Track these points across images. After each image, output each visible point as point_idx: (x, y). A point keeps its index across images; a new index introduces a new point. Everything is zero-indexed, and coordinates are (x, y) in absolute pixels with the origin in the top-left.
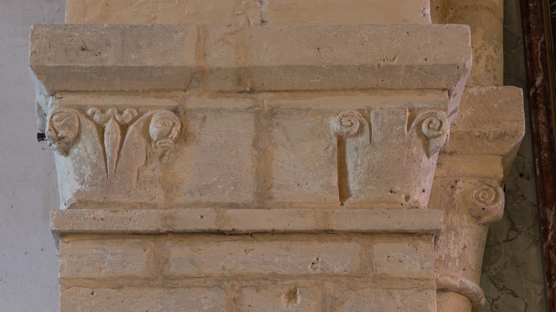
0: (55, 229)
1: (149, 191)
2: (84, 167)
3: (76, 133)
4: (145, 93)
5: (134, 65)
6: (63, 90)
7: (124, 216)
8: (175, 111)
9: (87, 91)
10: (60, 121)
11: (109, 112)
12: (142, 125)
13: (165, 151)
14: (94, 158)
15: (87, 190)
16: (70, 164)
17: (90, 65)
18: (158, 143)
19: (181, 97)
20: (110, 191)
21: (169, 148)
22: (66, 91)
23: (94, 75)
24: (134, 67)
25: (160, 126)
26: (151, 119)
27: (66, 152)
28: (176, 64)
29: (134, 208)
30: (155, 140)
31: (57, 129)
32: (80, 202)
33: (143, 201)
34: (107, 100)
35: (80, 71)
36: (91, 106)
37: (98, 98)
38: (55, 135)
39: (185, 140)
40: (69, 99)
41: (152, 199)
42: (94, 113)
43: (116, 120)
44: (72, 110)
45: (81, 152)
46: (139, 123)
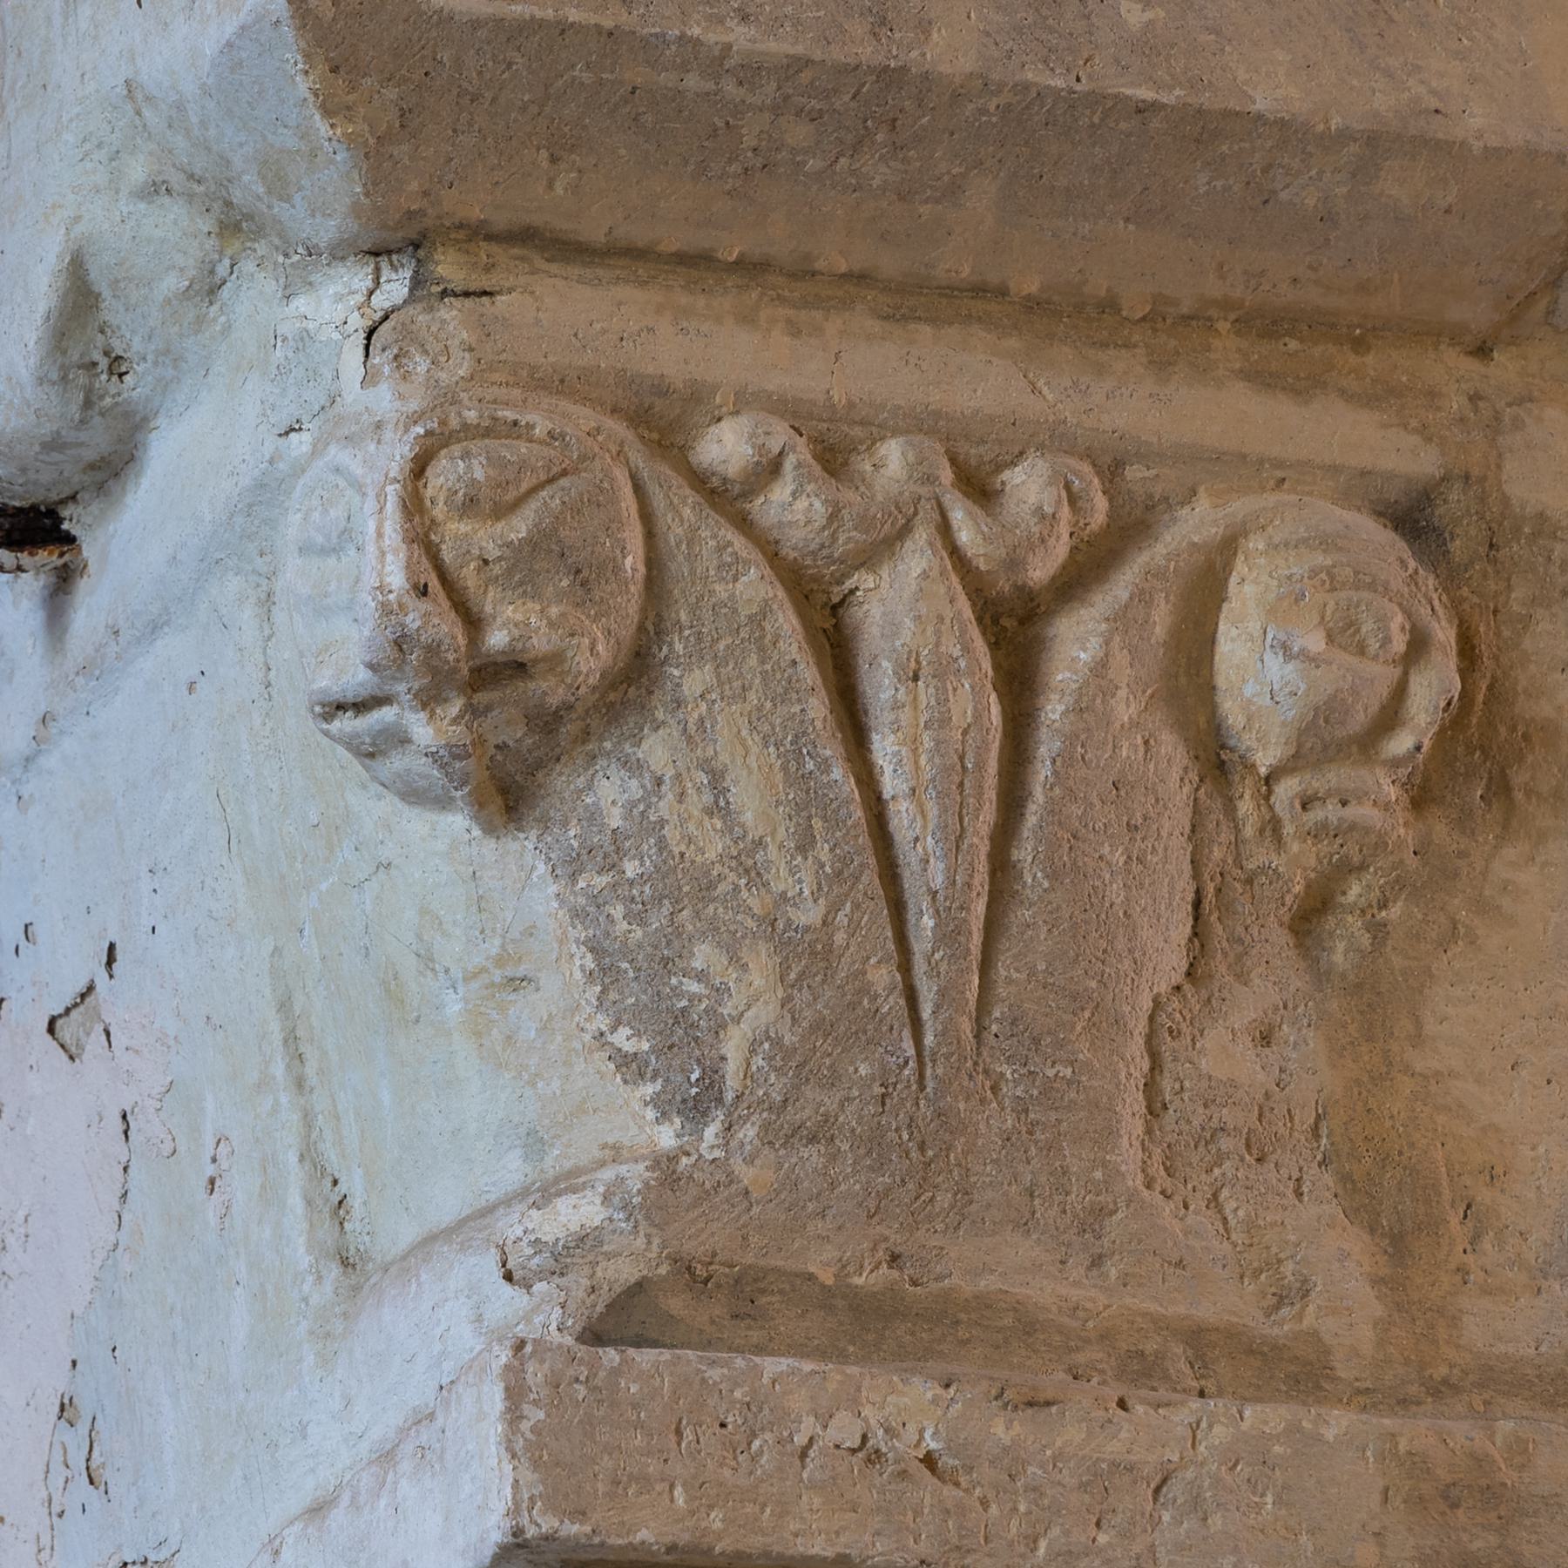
0: (548, 1524)
1: (1250, 1226)
2: (704, 955)
3: (627, 632)
4: (1172, 332)
5: (1145, 94)
6: (502, 220)
7: (1114, 1449)
8: (1412, 519)
9: (695, 263)
10: (501, 511)
11: (893, 460)
12: (1161, 619)
13: (1346, 869)
14: (796, 882)
15: (746, 1174)
16: (543, 900)
17: (779, 47)
18: (1287, 789)
19: (1456, 403)
20: (944, 1200)
21: (1381, 845)
22: (525, 237)
23: (799, 133)
24: (1143, 109)
25: (1315, 642)
26: (1228, 567)
27: (507, 794)
28: (1477, 121)
29: (1142, 1369)
30: (1264, 760)
31: (469, 577)
32: (692, 1275)
33: (1206, 1312)
34: (864, 364)
35: (692, 82)
36: (743, 401)
37: (794, 331)
38: (462, 641)
39: (1500, 788)
40: (558, 312)
41: (1281, 1300)
42: (773, 468)
43: (955, 552)
44: (585, 417)
45: (665, 806)
46: (1142, 597)
